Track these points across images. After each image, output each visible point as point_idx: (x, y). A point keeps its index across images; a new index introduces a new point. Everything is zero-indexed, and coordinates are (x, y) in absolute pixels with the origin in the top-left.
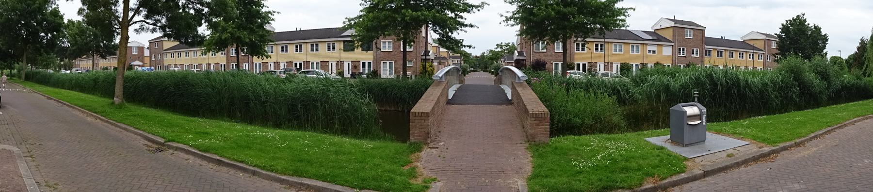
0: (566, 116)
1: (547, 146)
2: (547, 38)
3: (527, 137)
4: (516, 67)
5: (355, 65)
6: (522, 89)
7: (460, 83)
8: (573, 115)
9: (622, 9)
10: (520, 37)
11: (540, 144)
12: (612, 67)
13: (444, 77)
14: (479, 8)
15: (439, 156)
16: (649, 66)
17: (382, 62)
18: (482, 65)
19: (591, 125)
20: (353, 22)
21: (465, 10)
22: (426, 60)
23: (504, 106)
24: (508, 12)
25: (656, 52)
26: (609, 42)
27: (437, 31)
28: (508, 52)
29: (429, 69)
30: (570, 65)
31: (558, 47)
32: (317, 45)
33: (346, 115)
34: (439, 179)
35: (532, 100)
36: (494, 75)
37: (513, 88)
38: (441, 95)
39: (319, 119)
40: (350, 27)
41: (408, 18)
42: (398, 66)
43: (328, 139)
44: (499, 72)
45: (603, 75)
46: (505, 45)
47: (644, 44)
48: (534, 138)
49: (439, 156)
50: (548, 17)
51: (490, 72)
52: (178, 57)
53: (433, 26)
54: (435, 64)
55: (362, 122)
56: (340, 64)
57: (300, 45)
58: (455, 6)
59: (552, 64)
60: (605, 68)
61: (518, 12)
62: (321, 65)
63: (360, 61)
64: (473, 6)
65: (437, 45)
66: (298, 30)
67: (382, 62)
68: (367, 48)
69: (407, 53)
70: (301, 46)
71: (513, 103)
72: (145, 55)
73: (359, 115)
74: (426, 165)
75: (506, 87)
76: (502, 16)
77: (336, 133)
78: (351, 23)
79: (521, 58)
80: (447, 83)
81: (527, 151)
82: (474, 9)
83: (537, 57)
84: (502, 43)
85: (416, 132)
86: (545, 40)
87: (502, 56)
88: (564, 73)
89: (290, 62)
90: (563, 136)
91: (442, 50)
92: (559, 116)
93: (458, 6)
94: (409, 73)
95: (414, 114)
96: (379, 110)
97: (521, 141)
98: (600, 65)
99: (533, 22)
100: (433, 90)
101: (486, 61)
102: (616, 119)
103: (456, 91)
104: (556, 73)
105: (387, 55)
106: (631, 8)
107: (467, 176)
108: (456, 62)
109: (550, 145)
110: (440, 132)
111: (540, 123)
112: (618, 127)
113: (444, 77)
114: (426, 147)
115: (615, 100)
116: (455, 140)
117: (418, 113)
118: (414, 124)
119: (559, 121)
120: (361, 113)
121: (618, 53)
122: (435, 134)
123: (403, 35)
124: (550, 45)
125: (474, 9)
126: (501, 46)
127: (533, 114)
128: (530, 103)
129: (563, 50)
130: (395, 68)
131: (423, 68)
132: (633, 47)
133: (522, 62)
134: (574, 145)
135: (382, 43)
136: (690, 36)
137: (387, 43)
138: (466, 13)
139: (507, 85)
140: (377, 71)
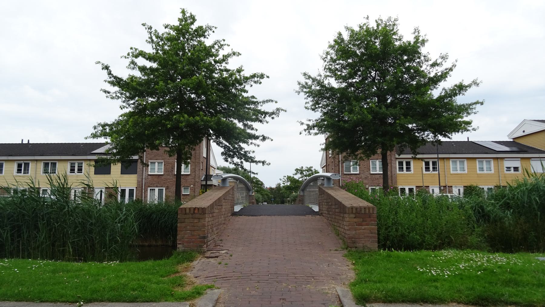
2: (359, 152)
14: (274, 116)
17: (149, 189)
24: (310, 120)
25: (520, 169)
26: (444, 158)
32: (54, 165)
34: (216, 286)
41: (184, 124)
42: (170, 194)
46: (306, 170)
47: (497, 158)
57: (25, 163)
59: (367, 189)
64: (265, 113)
66: (24, 142)
67: (149, 189)
69: (182, 177)
70: (27, 165)
74: (200, 273)
76: (302, 124)
81: (346, 258)
84: (302, 167)
85: (186, 236)
107: (260, 281)
110: (221, 240)
111: (363, 221)
117: (190, 208)
118: (183, 225)
124: (363, 160)
126: (301, 170)
129: (383, 171)
137: (156, 164)
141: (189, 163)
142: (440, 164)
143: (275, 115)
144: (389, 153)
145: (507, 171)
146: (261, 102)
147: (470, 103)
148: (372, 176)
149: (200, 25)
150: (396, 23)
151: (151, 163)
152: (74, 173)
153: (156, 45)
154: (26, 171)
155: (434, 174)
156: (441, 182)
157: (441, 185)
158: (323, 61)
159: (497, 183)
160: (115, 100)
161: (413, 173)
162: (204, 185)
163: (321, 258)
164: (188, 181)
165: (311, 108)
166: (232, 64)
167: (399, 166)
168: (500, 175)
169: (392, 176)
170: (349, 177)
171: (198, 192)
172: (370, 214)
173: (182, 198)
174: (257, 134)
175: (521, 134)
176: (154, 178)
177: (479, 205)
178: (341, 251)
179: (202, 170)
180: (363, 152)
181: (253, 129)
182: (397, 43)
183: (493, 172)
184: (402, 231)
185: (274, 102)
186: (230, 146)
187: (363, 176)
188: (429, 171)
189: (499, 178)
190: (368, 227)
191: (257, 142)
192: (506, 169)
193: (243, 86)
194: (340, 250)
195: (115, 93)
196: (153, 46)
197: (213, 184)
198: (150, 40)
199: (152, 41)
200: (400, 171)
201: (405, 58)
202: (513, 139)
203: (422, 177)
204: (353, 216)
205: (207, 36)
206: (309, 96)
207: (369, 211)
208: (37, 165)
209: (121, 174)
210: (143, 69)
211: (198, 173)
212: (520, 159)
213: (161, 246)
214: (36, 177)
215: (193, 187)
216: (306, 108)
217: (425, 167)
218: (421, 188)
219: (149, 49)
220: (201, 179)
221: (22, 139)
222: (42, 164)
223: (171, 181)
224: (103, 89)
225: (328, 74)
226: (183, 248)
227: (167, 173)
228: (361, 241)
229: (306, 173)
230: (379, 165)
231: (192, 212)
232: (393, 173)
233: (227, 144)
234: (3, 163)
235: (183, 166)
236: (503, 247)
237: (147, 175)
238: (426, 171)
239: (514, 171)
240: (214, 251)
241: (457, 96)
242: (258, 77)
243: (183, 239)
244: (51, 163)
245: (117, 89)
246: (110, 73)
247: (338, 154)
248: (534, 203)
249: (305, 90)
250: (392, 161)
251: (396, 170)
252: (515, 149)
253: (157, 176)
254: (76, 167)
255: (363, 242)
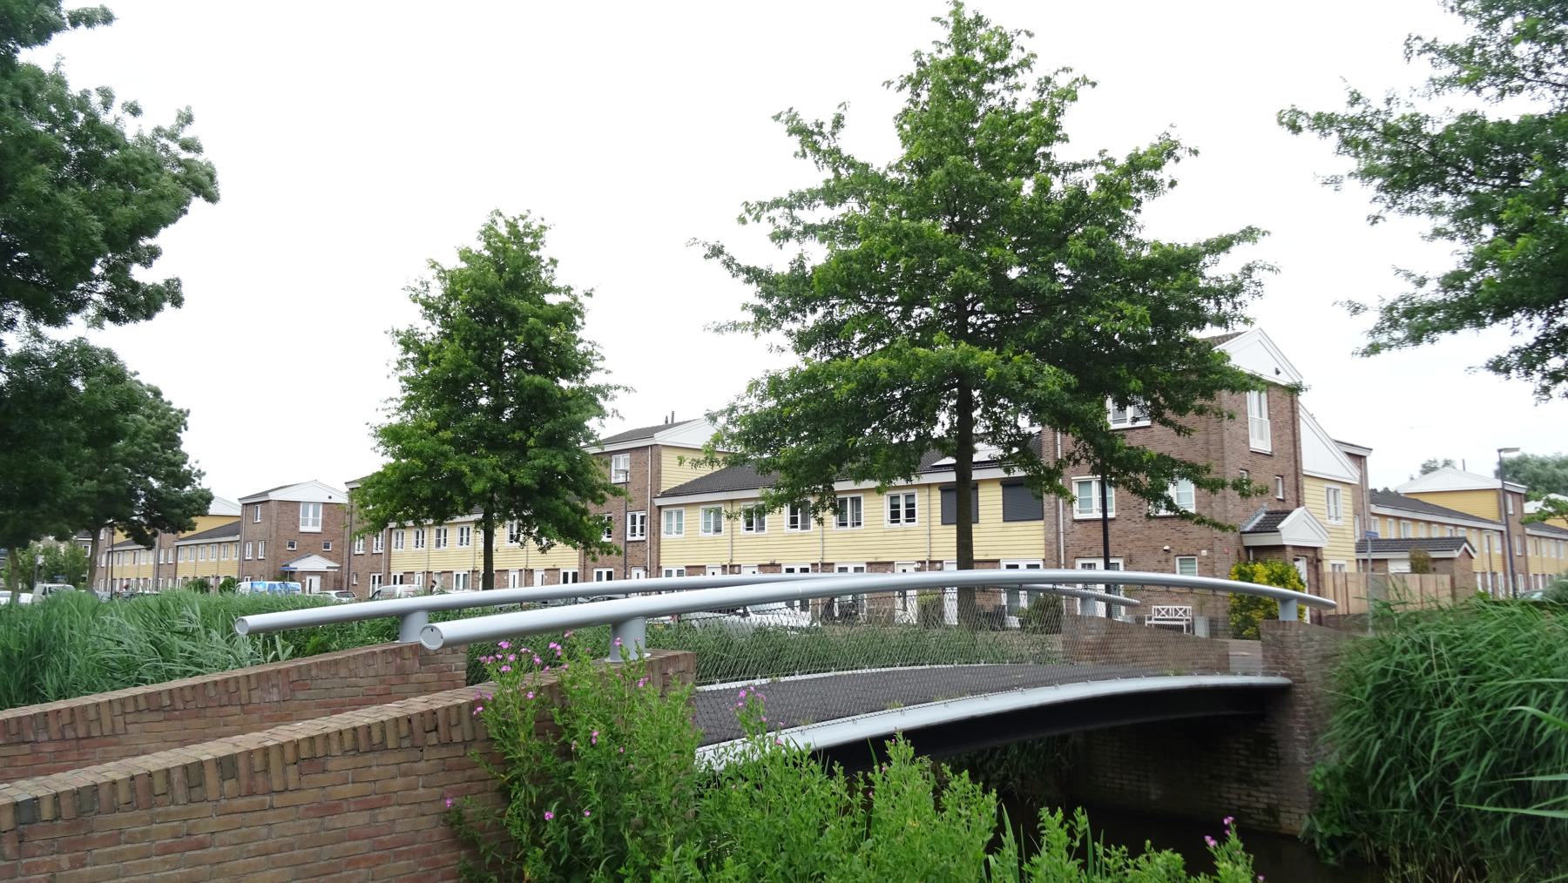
52: (438, 545)
57: (852, 499)
136: (315, 524)
149: (203, 146)
151: (1079, 483)
152: (898, 521)
164: (1189, 536)
176: (1090, 530)
197: (1285, 543)
208: (932, 498)
209: (1005, 520)
211: (1218, 509)
215: (1207, 557)
223: (1139, 539)
227: (1126, 513)
237: (1070, 523)
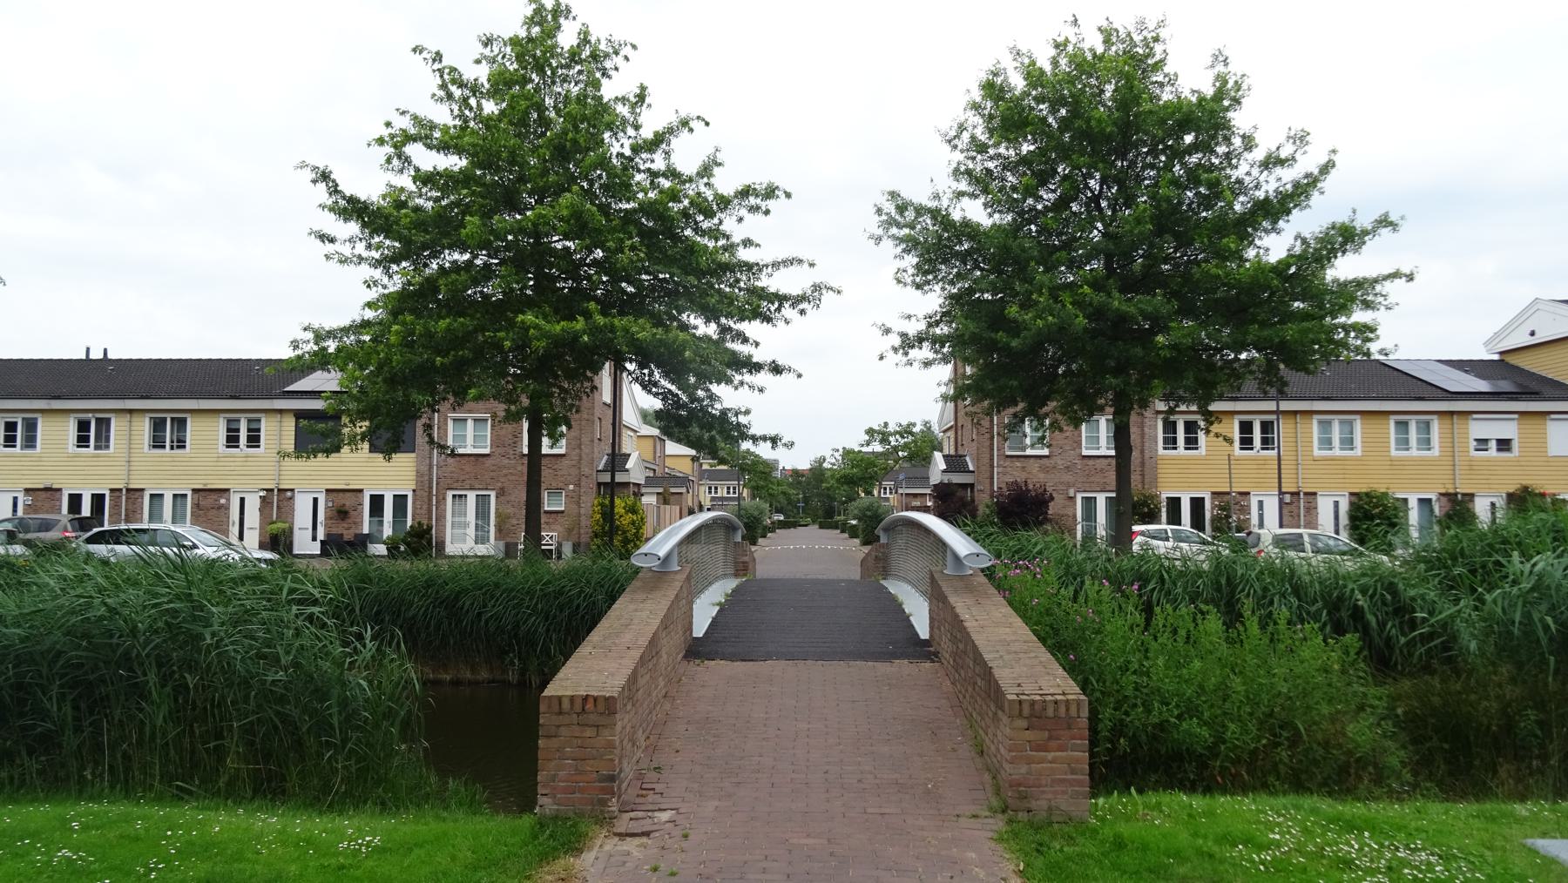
0: (1148, 711)
1: (1083, 834)
2: (1052, 405)
3: (998, 793)
4: (942, 515)
5: (342, 504)
6: (970, 601)
7: (736, 575)
8: (1177, 706)
9: (1360, 284)
10: (951, 405)
11: (1051, 824)
12: (1312, 509)
13: (675, 559)
14: (804, 305)
15: (655, 869)
16: (1481, 508)
17: (450, 494)
18: (815, 502)
19: (1254, 752)
20: (332, 346)
21: (757, 314)
22: (612, 488)
23: (902, 667)
24: (909, 317)
25: (1515, 445)
26: (1295, 413)
27: (656, 384)
28: (910, 458)
29: (627, 520)
30: (1145, 504)
31: (1097, 438)
32: (180, 424)
33: (278, 713)
35: (1015, 647)
36: (857, 541)
37: (937, 598)
38: (666, 624)
39: (153, 737)
40: (321, 361)
42: (510, 510)
43: (180, 827)
44: (879, 531)
45: (1279, 541)
46: (897, 433)
47: (1452, 413)
48: (1023, 797)
49: (655, 869)
50: (1059, 334)
51: (844, 528)
53: (642, 366)
54: (649, 500)
55: (345, 741)
56: (277, 500)
57: (98, 420)
58: (717, 297)
59: (1072, 499)
60: (1285, 511)
61: (946, 316)
62: (196, 506)
63: (361, 491)
64: (781, 299)
65: (656, 432)
66: (92, 356)
67: (450, 494)
68: (389, 441)
69: (544, 461)
70: (104, 424)
71: (936, 654)
72: (1410, 523)
73: (335, 710)
75: (907, 588)
76: (887, 331)
77: (231, 794)
78: (325, 349)
79: (957, 479)
80: (688, 578)
81: (1000, 847)
82: (787, 311)
83: (1016, 474)
84: (886, 424)
86: (1046, 415)
87: (887, 471)
88: (1120, 536)
89: (47, 489)
90: (1140, 791)
91: (672, 448)
92: (1115, 709)
93: (731, 299)
94: (550, 538)
95: (555, 703)
96: (424, 683)
97: (973, 809)
98: (1261, 503)
99: (1005, 350)
100: (632, 607)
101: (828, 489)
102: (1361, 732)
103: (723, 609)
104: (1089, 536)
105: (468, 468)
106: (1395, 275)
108: (722, 492)
109: (1095, 831)
111: (1050, 738)
112: (1371, 769)
113: (675, 559)
114: (604, 833)
115: (1352, 652)
116: (716, 803)
117: (572, 698)
118: (554, 743)
119: (1119, 729)
120: (344, 703)
121: (1337, 452)
122: (640, 776)
123: (531, 398)
124: (1061, 430)
125: (787, 311)
126: (883, 434)
127: (1020, 702)
128: (1006, 657)
129: (1116, 448)
130: (498, 515)
131: (603, 514)
132: (1403, 426)
133: (960, 493)
134: (1195, 835)
135: (450, 424)
137: (470, 423)
138: (756, 323)
139: (909, 582)
140: (430, 528)
141: (562, 435)
142: (1284, 429)
143: (809, 302)
144: (1134, 418)
145: (1477, 450)
146: (767, 266)
147: (1374, 276)
148: (1085, 461)
150: (1163, 33)
152: (238, 447)
153: (460, 107)
154: (103, 441)
155: (1265, 459)
156: (1283, 480)
157: (1284, 490)
158: (948, 148)
159: (1447, 486)
160: (352, 265)
161: (1204, 453)
162: (605, 484)
163: (932, 850)
165: (914, 282)
166: (686, 155)
167: (1164, 433)
168: (1457, 463)
169: (1143, 464)
170: (1018, 464)
171: (589, 504)
172: (1070, 718)
173: (542, 521)
174: (758, 356)
175: (1523, 340)
177: (1386, 582)
178: (986, 821)
179: (599, 440)
180: (1061, 407)
181: (745, 340)
182: (1167, 96)
183: (1436, 452)
184: (1160, 713)
185: (806, 265)
186: (679, 392)
187: (1060, 462)
188: (1252, 449)
189: (1454, 470)
190: (1064, 754)
191: (763, 378)
192: (1475, 443)
193: (716, 221)
194: (986, 817)
195: (350, 241)
196: (452, 111)
197: (632, 481)
198: (442, 93)
199: (450, 96)
200: (1168, 449)
201: (1189, 139)
202: (1501, 353)
203: (1233, 471)
204: (1023, 723)
205: (612, 73)
206: (907, 251)
207: (1067, 710)
208: (133, 424)
210: (426, 179)
212: (1516, 416)
213: (489, 683)
214: (132, 459)
216: (899, 281)
217: (1241, 439)
218: (1226, 498)
219: (443, 115)
220: (598, 466)
221: (89, 345)
222: (147, 420)
224: (314, 230)
225: (963, 186)
226: (555, 807)
227: (500, 450)
228: (1043, 792)
229: (897, 441)
230: (1108, 432)
231: (578, 707)
232: (1147, 456)
233: (673, 388)
234: (36, 419)
235: (546, 441)
236: (1446, 746)
238: (1241, 449)
239: (1499, 450)
240: (640, 814)
241: (1336, 257)
242: (758, 196)
243: (554, 781)
244: (172, 419)
245: (353, 228)
246: (335, 190)
247: (989, 414)
248: (1541, 633)
249: (894, 230)
250: (1146, 420)
251: (1156, 445)
252: (1505, 386)
253: (472, 458)
254: (241, 431)
255: (1050, 796)
